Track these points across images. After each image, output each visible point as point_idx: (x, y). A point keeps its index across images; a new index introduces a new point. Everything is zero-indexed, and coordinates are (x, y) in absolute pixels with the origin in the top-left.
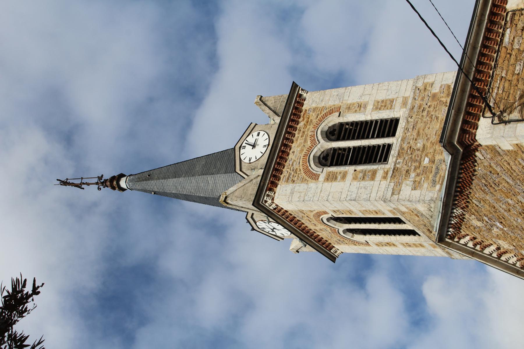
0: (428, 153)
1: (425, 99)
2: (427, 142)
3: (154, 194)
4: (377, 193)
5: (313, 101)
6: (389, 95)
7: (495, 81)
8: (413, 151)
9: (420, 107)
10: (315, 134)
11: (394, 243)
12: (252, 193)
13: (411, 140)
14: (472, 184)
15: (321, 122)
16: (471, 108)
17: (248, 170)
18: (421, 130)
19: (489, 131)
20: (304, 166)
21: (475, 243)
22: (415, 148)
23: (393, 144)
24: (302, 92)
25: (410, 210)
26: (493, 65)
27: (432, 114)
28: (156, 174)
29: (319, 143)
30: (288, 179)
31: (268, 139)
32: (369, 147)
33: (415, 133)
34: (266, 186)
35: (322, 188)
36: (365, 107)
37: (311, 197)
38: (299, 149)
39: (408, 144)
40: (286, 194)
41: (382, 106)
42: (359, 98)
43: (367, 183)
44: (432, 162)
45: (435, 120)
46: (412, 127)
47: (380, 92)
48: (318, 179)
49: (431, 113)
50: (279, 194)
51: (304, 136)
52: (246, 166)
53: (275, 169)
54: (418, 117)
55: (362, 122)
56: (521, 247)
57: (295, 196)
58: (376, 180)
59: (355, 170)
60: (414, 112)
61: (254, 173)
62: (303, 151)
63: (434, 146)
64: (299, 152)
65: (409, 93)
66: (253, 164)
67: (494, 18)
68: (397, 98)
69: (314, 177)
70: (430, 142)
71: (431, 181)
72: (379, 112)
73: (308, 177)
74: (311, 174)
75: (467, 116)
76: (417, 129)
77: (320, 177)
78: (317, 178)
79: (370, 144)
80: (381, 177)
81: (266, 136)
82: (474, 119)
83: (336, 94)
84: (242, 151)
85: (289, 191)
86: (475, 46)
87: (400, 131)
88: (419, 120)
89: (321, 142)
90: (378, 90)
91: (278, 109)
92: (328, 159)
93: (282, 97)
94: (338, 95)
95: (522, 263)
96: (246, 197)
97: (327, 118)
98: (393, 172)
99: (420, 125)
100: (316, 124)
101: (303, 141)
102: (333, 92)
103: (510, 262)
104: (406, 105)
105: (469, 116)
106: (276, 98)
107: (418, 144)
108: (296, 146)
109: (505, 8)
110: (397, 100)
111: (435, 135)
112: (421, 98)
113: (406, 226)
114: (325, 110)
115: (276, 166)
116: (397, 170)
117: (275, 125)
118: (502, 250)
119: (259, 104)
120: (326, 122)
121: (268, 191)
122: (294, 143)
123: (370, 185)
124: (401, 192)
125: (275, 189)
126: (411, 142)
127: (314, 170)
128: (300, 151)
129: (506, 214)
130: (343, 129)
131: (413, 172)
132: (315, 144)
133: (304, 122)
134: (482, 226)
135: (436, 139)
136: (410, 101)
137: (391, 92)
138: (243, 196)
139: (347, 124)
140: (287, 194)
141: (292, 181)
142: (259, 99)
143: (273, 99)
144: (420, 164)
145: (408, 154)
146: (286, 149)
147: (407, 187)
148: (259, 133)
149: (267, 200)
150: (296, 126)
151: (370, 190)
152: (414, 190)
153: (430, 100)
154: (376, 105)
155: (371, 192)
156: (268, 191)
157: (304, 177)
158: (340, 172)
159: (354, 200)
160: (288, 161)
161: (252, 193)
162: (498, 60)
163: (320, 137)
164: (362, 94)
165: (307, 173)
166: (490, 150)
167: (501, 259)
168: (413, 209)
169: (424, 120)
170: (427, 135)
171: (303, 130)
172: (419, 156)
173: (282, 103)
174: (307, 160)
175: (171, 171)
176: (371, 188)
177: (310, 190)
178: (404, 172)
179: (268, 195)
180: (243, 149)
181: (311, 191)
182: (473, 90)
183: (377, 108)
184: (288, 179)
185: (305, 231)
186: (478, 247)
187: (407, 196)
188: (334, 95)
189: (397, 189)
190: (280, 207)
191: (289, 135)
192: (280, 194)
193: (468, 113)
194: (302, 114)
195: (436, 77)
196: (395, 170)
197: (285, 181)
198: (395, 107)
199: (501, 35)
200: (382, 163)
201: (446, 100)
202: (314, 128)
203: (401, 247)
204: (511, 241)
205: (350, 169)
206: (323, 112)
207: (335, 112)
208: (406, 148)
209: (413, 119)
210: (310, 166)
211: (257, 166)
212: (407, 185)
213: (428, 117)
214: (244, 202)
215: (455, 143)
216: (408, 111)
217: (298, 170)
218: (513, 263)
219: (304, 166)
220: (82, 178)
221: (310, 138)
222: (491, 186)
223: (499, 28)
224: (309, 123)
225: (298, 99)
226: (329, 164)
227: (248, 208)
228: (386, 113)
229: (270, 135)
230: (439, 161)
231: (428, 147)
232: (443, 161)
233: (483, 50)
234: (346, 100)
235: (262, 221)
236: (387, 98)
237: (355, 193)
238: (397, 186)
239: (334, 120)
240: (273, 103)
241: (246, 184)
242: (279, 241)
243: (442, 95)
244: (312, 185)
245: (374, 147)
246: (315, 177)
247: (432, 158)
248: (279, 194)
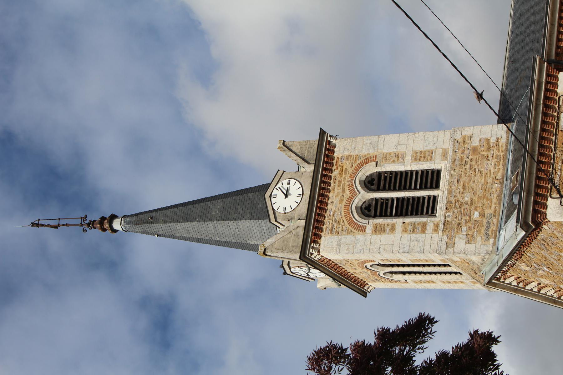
0: (476, 207)
1: (465, 152)
2: (474, 196)
3: (158, 236)
4: (430, 246)
5: (345, 149)
6: (427, 146)
7: (557, 163)
8: (461, 204)
9: (461, 160)
10: (353, 184)
11: (434, 281)
12: (293, 245)
13: (458, 194)
14: (531, 243)
15: (357, 171)
16: (539, 189)
17: (285, 220)
18: (466, 184)
19: (558, 211)
20: (347, 217)
21: (518, 281)
22: (463, 202)
23: (438, 196)
24: (331, 138)
25: (463, 260)
26: (553, 148)
27: (475, 168)
28: (160, 216)
29: (360, 193)
30: (332, 230)
31: (301, 188)
32: (413, 198)
33: (460, 187)
34: (310, 239)
35: (371, 240)
36: (403, 158)
37: (360, 250)
38: (338, 199)
39: (455, 197)
40: (332, 246)
41: (421, 157)
42: (395, 148)
43: (418, 236)
44: (483, 216)
45: (479, 174)
46: (456, 180)
47: (417, 143)
48: (365, 231)
49: (474, 167)
50: (324, 245)
51: (342, 185)
52: (281, 216)
53: (316, 221)
54: (461, 170)
55: (401, 172)
56: (561, 283)
57: (342, 248)
58: (427, 233)
59: (404, 223)
60: (456, 166)
61: (292, 224)
62: (343, 201)
63: (482, 200)
64: (338, 203)
65: (448, 145)
66: (288, 214)
67: (549, 103)
68: (436, 149)
69: (360, 228)
70: (477, 196)
71: (484, 234)
72: (419, 164)
73: (354, 228)
74: (356, 226)
75: (536, 197)
76: (462, 182)
77: (367, 229)
78: (364, 230)
79: (414, 196)
80: (431, 230)
81: (298, 185)
82: (543, 200)
83: (368, 142)
84: (273, 200)
85: (335, 244)
86: (534, 129)
87: (444, 184)
88: (463, 173)
89: (361, 193)
90: (414, 140)
91: (306, 155)
92: (371, 210)
93: (308, 142)
94: (371, 143)
95: (559, 294)
96: (287, 249)
97: (363, 167)
98: (444, 225)
99: (464, 179)
100: (353, 173)
101: (341, 191)
102: (365, 140)
103: (549, 294)
104: (446, 157)
105: (538, 197)
106: (302, 144)
107: (466, 198)
108: (334, 196)
109: (556, 92)
110: (436, 151)
111: (482, 189)
112: (461, 151)
113: (452, 269)
114: (359, 159)
115: (316, 217)
116: (448, 224)
117: (306, 173)
118: (542, 285)
119: (283, 149)
120: (363, 171)
121: (313, 244)
122: (331, 193)
123: (421, 237)
124: (456, 246)
125: (319, 240)
126: (458, 195)
127: (359, 222)
128: (339, 201)
129: (555, 262)
130: (382, 179)
131: (465, 225)
132: (355, 195)
133: (339, 170)
134: (529, 270)
135: (482, 193)
136: (450, 153)
137: (428, 143)
138: (284, 248)
139: (386, 172)
140: (333, 246)
141: (336, 233)
142: (282, 144)
143: (298, 145)
144: (470, 217)
145: (456, 207)
146: (324, 200)
147: (461, 240)
148: (290, 181)
149: (313, 252)
150: (330, 175)
151: (423, 243)
152: (469, 243)
153: (470, 153)
154: (415, 156)
155: (424, 245)
156: (313, 244)
157: (349, 228)
158: (387, 224)
159: (407, 253)
160: (328, 212)
161: (294, 245)
162: (557, 143)
163: (359, 188)
164: (398, 143)
165: (351, 224)
166: (557, 224)
167: (541, 292)
168: (467, 259)
169: (468, 173)
170: (473, 189)
171: (339, 179)
172: (469, 210)
173: (309, 149)
174: (349, 211)
175: (180, 213)
176: (423, 240)
177: (358, 242)
178: (455, 226)
179: (313, 248)
180: (274, 198)
181: (360, 243)
182: (539, 172)
183: (416, 159)
184: (332, 230)
185: (344, 274)
186: (521, 285)
187: (462, 250)
188: (367, 143)
189: (451, 242)
190: (324, 257)
191: (325, 184)
192: (325, 246)
193: (537, 194)
194: (334, 162)
195: (473, 130)
196: (446, 223)
197: (329, 233)
198: (435, 158)
199: (556, 118)
200: (430, 216)
201: (488, 154)
202: (351, 177)
203: (440, 283)
204: (553, 279)
205: (398, 221)
206: (357, 161)
207: (371, 161)
208: (453, 201)
209: (456, 172)
210: (354, 217)
211: (294, 217)
212: (460, 239)
213: (471, 171)
214: (286, 254)
215: (530, 223)
216: (449, 163)
217: (341, 221)
218: (551, 295)
219: (347, 217)
220: (59, 219)
221: (348, 187)
222: (548, 245)
223: (554, 112)
224: (344, 172)
225: (328, 146)
226: (373, 215)
227: (288, 258)
228: (427, 165)
229: (302, 183)
230: (488, 215)
231: (476, 201)
232: (493, 215)
233: (543, 134)
234: (381, 149)
235: (298, 267)
236: (426, 149)
237: (407, 246)
238: (450, 239)
239: (370, 169)
240: (299, 149)
241: (285, 235)
242: (310, 281)
243: (482, 149)
244: (360, 237)
245: (419, 198)
246: (362, 229)
247: (481, 212)
248: (324, 245)
